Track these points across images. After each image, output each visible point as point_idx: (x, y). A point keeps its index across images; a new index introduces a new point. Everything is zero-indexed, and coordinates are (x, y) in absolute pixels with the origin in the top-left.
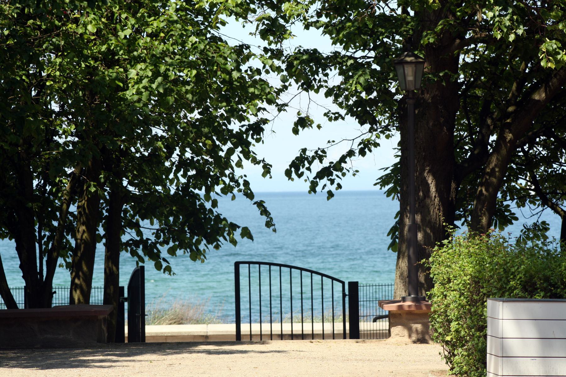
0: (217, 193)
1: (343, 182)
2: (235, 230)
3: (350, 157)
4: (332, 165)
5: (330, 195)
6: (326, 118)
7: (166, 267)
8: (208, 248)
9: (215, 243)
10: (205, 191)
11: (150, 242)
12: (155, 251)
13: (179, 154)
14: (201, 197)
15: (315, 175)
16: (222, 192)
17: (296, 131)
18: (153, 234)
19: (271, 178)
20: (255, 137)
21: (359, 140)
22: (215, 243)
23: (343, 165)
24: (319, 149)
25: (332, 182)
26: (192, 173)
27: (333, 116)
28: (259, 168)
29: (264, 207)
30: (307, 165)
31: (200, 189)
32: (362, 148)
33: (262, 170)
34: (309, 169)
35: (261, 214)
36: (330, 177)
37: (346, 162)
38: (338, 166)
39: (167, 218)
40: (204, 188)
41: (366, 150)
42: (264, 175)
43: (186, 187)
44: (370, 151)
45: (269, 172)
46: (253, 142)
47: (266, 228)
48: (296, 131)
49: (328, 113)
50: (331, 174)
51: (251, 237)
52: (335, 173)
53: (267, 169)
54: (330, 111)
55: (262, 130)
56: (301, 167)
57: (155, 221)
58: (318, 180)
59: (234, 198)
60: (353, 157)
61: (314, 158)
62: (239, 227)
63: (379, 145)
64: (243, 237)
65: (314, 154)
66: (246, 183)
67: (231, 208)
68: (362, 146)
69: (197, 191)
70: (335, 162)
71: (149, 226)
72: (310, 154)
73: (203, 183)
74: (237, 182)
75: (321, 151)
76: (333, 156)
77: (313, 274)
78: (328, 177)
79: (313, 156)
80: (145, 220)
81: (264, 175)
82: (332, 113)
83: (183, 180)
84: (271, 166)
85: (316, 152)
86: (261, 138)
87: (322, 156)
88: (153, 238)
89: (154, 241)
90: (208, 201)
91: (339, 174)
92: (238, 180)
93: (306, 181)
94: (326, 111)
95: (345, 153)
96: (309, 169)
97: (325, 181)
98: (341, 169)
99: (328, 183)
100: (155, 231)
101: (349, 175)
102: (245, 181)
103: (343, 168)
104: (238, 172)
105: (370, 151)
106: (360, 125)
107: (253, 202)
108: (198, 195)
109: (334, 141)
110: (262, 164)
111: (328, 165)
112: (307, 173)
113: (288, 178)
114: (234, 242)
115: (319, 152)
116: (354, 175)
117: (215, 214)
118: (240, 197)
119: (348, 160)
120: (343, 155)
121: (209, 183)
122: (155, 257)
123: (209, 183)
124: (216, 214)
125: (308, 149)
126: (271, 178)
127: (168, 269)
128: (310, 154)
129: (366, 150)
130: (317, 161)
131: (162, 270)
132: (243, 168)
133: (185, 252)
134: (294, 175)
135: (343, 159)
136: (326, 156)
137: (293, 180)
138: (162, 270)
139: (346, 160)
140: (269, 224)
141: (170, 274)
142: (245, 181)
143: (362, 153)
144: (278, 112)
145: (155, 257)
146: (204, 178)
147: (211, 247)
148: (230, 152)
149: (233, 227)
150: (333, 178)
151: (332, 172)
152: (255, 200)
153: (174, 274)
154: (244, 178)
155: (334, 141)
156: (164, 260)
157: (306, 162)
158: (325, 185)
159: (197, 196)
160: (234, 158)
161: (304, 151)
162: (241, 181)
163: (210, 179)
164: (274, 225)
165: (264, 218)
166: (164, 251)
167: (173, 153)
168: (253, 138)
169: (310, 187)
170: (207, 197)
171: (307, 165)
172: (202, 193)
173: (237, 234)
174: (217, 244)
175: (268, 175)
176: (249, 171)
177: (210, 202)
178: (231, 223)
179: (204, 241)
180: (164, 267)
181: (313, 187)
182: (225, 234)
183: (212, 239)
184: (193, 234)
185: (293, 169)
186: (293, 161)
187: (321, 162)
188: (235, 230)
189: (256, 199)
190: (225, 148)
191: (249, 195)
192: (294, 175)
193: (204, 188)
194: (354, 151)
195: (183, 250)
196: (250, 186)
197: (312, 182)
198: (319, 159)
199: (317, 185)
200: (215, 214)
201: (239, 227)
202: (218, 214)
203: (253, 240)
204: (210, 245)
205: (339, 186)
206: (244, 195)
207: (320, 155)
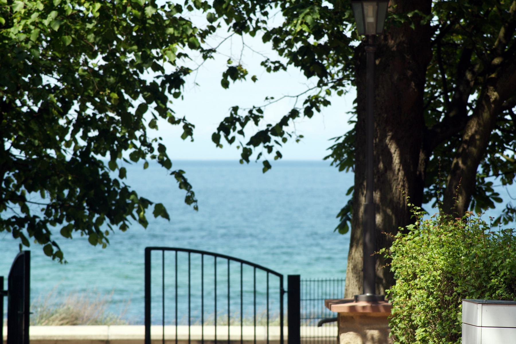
0: (125, 160)
1: (284, 149)
5: (267, 165)
6: (264, 69)
9: (121, 223)
11: (37, 220)
17: (225, 84)
18: (42, 210)
19: (192, 141)
20: (173, 91)
21: (305, 97)
22: (121, 223)
24: (254, 107)
25: (270, 149)
27: (273, 66)
28: (179, 129)
29: (183, 178)
31: (104, 155)
34: (241, 132)
41: (314, 110)
42: (184, 137)
43: (85, 153)
44: (318, 110)
45: (191, 134)
48: (225, 84)
49: (266, 61)
50: (268, 140)
51: (166, 216)
52: (273, 138)
53: (188, 130)
54: (268, 59)
55: (182, 82)
61: (247, 119)
62: (151, 203)
66: (162, 148)
67: (141, 179)
68: (308, 104)
69: (99, 157)
72: (242, 113)
74: (149, 146)
76: (271, 117)
81: (184, 137)
83: (82, 143)
84: (193, 126)
85: (250, 112)
88: (42, 216)
89: (42, 219)
91: (279, 139)
94: (264, 60)
95: (286, 113)
96: (241, 132)
97: (261, 148)
98: (281, 134)
99: (265, 150)
101: (291, 141)
104: (151, 134)
105: (318, 110)
109: (272, 98)
111: (264, 128)
114: (143, 222)
115: (255, 112)
116: (298, 141)
117: (122, 186)
125: (240, 107)
126: (192, 141)
127: (59, 255)
128: (242, 113)
129: (314, 110)
130: (251, 123)
132: (157, 129)
135: (284, 121)
136: (262, 117)
137: (221, 146)
140: (189, 200)
141: (61, 261)
143: (308, 113)
144: (202, 60)
146: (108, 141)
148: (142, 109)
149: (145, 203)
154: (159, 141)
155: (272, 98)
157: (238, 125)
158: (260, 154)
159: (99, 164)
160: (147, 117)
161: (235, 109)
162: (155, 146)
163: (116, 143)
165: (184, 193)
168: (170, 92)
170: (113, 165)
172: (106, 159)
175: (189, 137)
176: (166, 133)
179: (107, 220)
181: (246, 154)
185: (222, 133)
187: (256, 123)
189: (173, 169)
191: (166, 163)
192: (223, 140)
197: (245, 149)
200: (122, 186)
201: (151, 203)
205: (279, 155)
207: (255, 116)
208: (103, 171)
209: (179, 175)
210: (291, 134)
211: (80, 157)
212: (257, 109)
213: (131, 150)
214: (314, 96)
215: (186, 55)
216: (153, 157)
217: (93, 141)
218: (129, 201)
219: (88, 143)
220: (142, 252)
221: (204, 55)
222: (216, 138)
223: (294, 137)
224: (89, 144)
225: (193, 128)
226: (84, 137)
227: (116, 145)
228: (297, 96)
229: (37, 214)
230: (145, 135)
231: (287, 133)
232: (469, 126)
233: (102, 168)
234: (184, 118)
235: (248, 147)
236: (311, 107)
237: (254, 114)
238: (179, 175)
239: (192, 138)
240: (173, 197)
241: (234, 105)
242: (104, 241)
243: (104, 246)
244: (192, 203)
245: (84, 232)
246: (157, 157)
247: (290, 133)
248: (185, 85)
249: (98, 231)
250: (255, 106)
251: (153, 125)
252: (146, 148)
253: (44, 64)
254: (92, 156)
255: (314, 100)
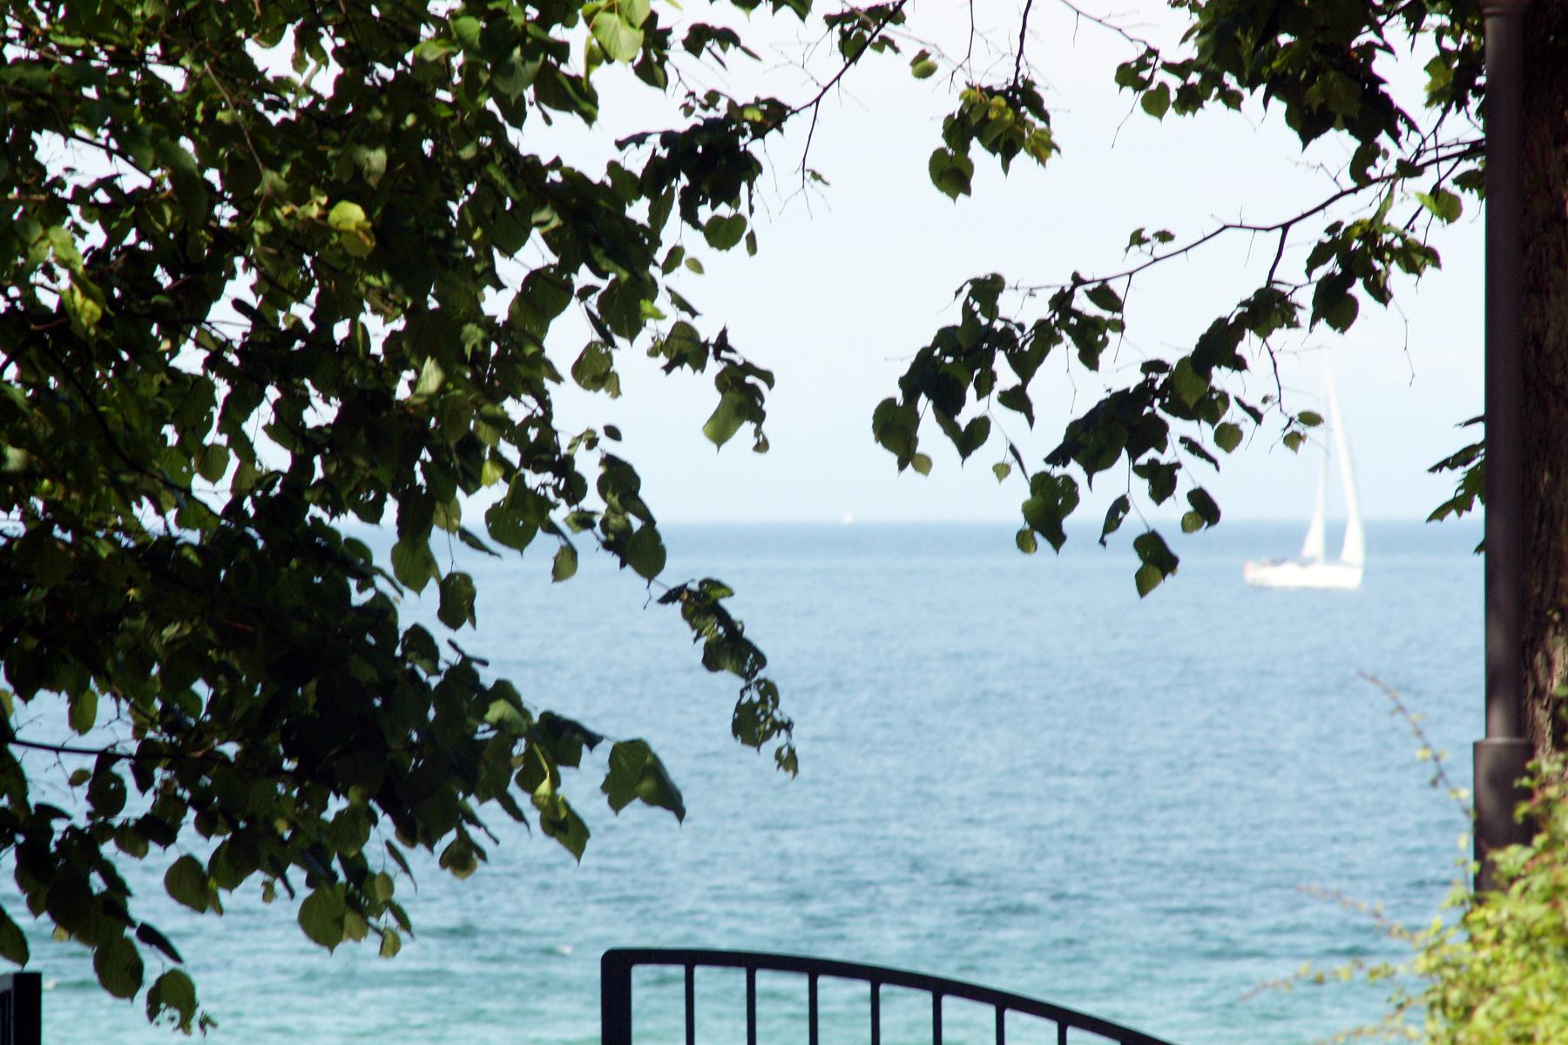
0: (467, 537)
1: (1227, 480)
2: (574, 761)
3: (1264, 333)
4: (1162, 379)
5: (1156, 558)
6: (1131, 97)
7: (160, 981)
8: (406, 869)
9: (451, 836)
10: (399, 522)
11: (59, 826)
12: (97, 883)
13: (253, 301)
14: (376, 562)
15: (1057, 439)
16: (495, 534)
17: (951, 174)
18: (76, 780)
19: (762, 446)
20: (705, 213)
21: (1312, 233)
22: (451, 836)
23: (1221, 378)
24: (1078, 280)
25: (1162, 481)
26: (321, 413)
27: (1174, 82)
28: (699, 390)
29: (724, 617)
30: (1005, 375)
31: (372, 514)
32: (1329, 278)
33: (714, 399)
34: (1017, 400)
35: (712, 661)
36: (1152, 453)
37: (1239, 364)
38: (1191, 384)
39: (176, 685)
40: (391, 507)
41: (1358, 289)
42: (720, 431)
43: (281, 505)
44: (1381, 294)
45: (758, 416)
46: (696, 243)
47: (736, 744)
48: (951, 174)
49: (1142, 63)
50: (1157, 435)
51: (668, 798)
52: (1178, 427)
53: (742, 396)
54: (1152, 52)
55: (749, 168)
56: (971, 392)
57: (106, 705)
58: (1074, 470)
59: (565, 564)
60: (1280, 336)
61: (1045, 335)
62: (593, 740)
63: (1432, 256)
64: (617, 803)
65: (1043, 312)
66: (621, 480)
67: (539, 626)
68: (1331, 266)
69: (348, 524)
70: (1172, 360)
71: (62, 733)
72: (1022, 309)
73: (384, 474)
74: (564, 467)
75: (1092, 295)
76: (1158, 330)
77: (1009, 1015)
78: (1134, 456)
79: (1041, 326)
80: (43, 695)
81: (720, 431)
82: (1168, 67)
83: (275, 457)
84: (768, 377)
85: (1061, 302)
86: (739, 221)
87: (1096, 325)
88: (77, 808)
89: (82, 822)
90: (418, 587)
91: (1203, 432)
92: (569, 461)
93: (1001, 471)
94: (1131, 54)
95: (1229, 307)
96: (1017, 400)
97: (1120, 478)
98: (1208, 406)
99: (1140, 489)
100: (90, 763)
101: (1260, 440)
102: (610, 461)
103: (1224, 397)
104: (574, 410)
105: (1381, 294)
106: (1293, 136)
107: (659, 588)
108: (357, 547)
109: (1165, 236)
110: (714, 367)
111: (1132, 379)
112: (1006, 422)
113: (892, 459)
114: (566, 828)
115: (1082, 303)
116: (1293, 440)
117: (448, 657)
118: (596, 560)
119: (1249, 345)
120: (1220, 323)
121: (420, 479)
122: (98, 920)
123: (420, 479)
124: (455, 659)
125: (1009, 281)
126: (762, 446)
127: (175, 996)
128: (1022, 309)
129: (1358, 289)
130: (1064, 353)
131: (142, 995)
132: (617, 393)
133: (269, 894)
134: (930, 435)
135: (1219, 345)
136: (1119, 326)
137: (924, 465)
138: (142, 995)
139: (1242, 349)
140: (753, 723)
141: (184, 1025)
142: (610, 461)
143: (1335, 306)
144: (838, 60)
145: (98, 920)
146: (386, 448)
147: (418, 857)
148: (544, 296)
149: (562, 739)
150: (1165, 459)
151: (1164, 427)
152: (670, 577)
153: (205, 1022)
154: (606, 445)
155: (1165, 236)
156: (150, 935)
157: (1001, 362)
158: (1121, 505)
159: (354, 560)
160: (568, 334)
161: (987, 290)
162: (588, 466)
163: (425, 455)
164: (788, 726)
165: (728, 686)
166: (145, 880)
167: (217, 294)
168: (689, 215)
169: (1027, 510)
170: (414, 562)
171: (1005, 375)
172: (380, 537)
173: (582, 785)
174: (465, 843)
175: (748, 428)
176: (649, 414)
177: (432, 591)
178: (548, 717)
179: (385, 827)
180: (151, 977)
181: (1048, 512)
182: (513, 789)
183: (428, 814)
184: (318, 781)
185: (925, 405)
186: (924, 356)
187: (1090, 357)
188: (574, 761)
189: (679, 570)
190: (514, 269)
191: (639, 548)
192: (930, 435)
193: (391, 507)
194: (1283, 297)
195: (257, 878)
196: (642, 494)
197: (1041, 483)
198: (1078, 340)
199: (1072, 500)
200: (448, 657)
201: (593, 740)
202: (467, 660)
203: (680, 813)
204: (421, 848)
205: (1204, 508)
206: (607, 546)
207: (1084, 321)
208: (369, 595)
209: (701, 602)
210: (1261, 408)
211: (256, 522)
212: (1090, 287)
213: (494, 492)
214: (1357, 224)
215: (727, 37)
216: (584, 521)
217: (318, 450)
218: (484, 733)
219: (295, 458)
220: (594, 973)
221: (845, 36)
222: (894, 428)
223: (1274, 422)
224: (302, 464)
225: (762, 385)
226: (287, 428)
227: (425, 467)
228: (1285, 227)
229: (53, 799)
230: (544, 421)
231: (1238, 400)
232: (75, 310)
233: (366, 577)
234: (723, 335)
235: (1058, 471)
236: (1347, 279)
237: (1077, 314)
238: (701, 602)
239: (758, 432)
240: (683, 712)
241: (982, 272)
242: (387, 920)
243: (390, 947)
244: (767, 736)
245: (278, 885)
246: (598, 519)
247: (1253, 400)
248: (760, 180)
249: (359, 871)
250: (1085, 275)
251: (595, 371)
252: (548, 477)
253: (19, 82)
254: (317, 521)
255: (1356, 244)
